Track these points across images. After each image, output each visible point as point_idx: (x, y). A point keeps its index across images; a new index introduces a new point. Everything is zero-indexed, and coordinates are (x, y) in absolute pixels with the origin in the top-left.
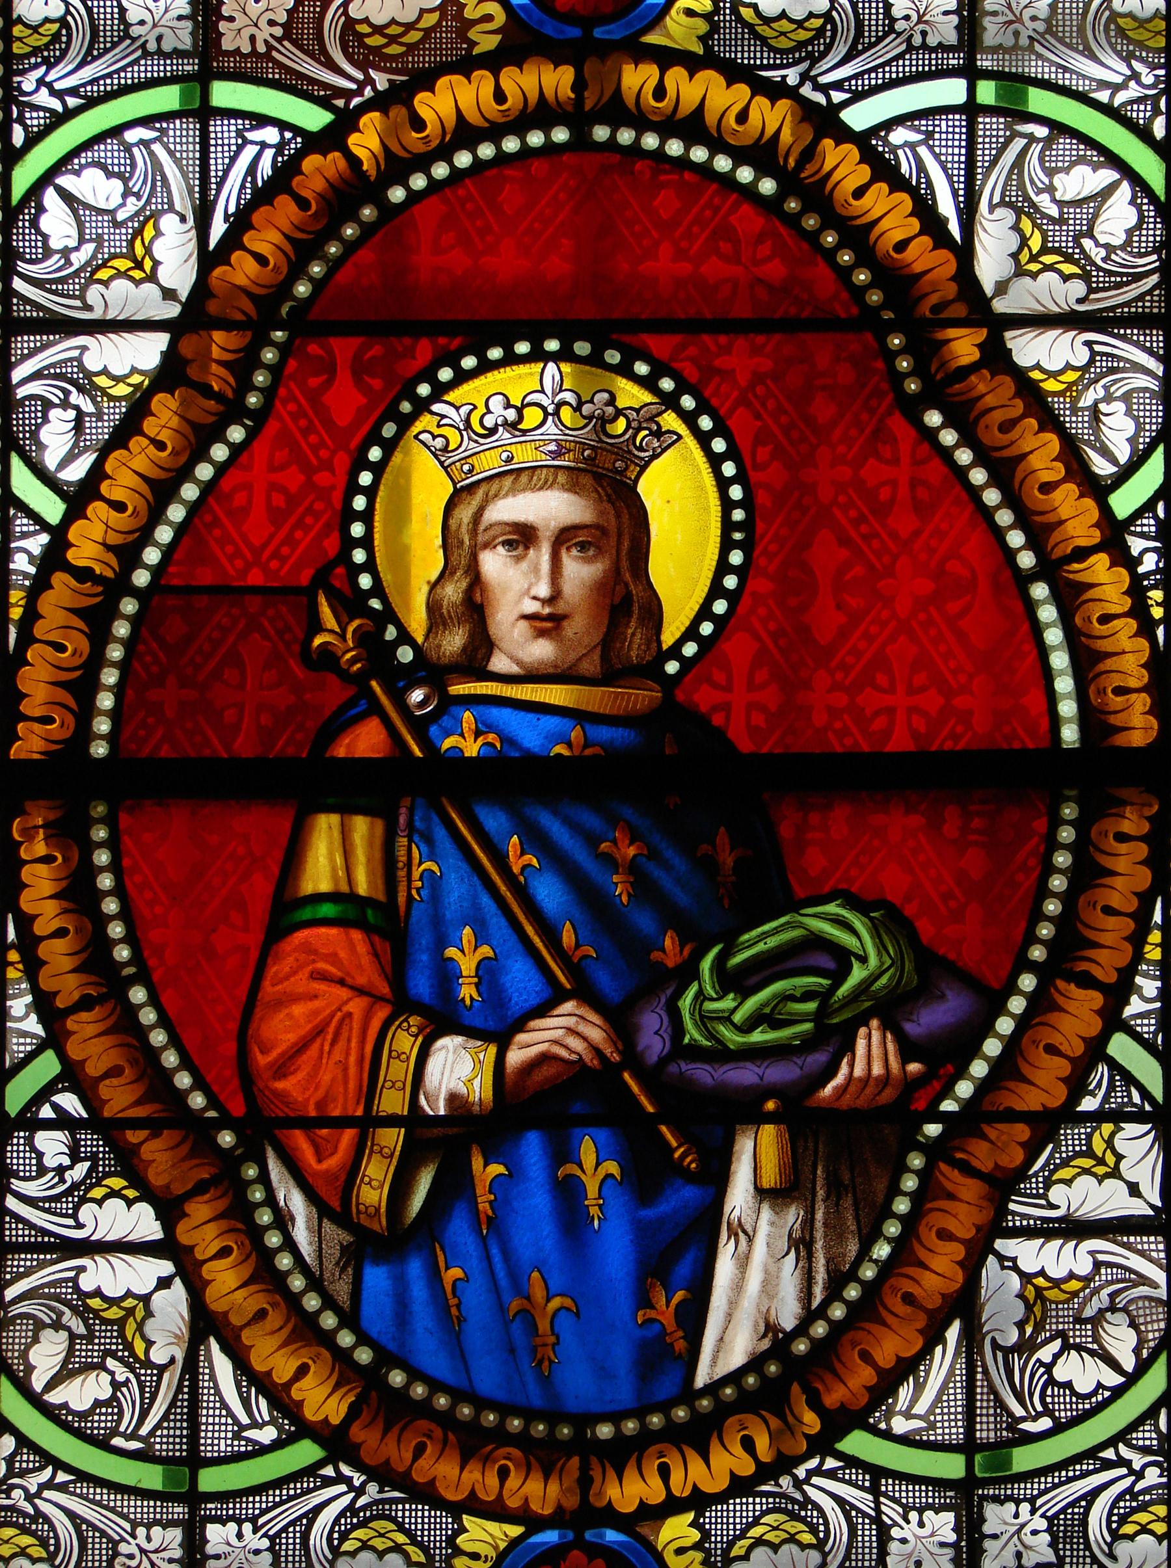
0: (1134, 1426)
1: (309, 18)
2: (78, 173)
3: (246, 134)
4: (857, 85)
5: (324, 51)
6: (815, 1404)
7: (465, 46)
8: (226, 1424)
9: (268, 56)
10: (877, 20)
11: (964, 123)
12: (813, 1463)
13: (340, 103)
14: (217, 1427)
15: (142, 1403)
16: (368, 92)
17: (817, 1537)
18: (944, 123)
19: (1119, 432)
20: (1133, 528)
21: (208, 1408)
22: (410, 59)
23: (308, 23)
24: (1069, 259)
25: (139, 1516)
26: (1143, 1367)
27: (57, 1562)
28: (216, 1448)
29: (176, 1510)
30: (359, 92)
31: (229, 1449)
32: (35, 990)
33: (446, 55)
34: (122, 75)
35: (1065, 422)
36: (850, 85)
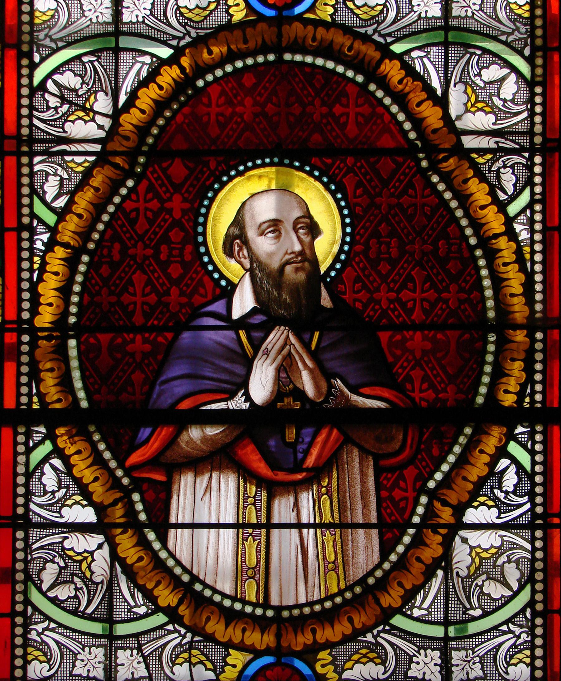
0: (48, 56)
1: (402, 665)
2: (503, 596)
3: (427, 613)
4: (162, 632)
5: (395, 651)
6: (182, 69)
7: (333, 653)
8: (125, 606)
9: (420, 648)
10: (153, 662)
11: (114, 616)
12: (182, 43)
13: (387, 628)
14: (121, 607)
15: (468, 67)
16: (375, 632)
17: (180, 11)
18: (123, 616)
19: (50, 479)
20: (43, 436)
21: (117, 599)
22: (357, 647)
23: (402, 663)
24: (70, 557)
25: (86, 642)
26: (521, 588)
27: (505, 2)
28: (120, 616)
29: (455, 23)
30: (379, 632)
31: (126, 616)
32: (518, 243)
33: (341, 649)
34: (483, 640)
35: (72, 482)
36: (165, 632)
